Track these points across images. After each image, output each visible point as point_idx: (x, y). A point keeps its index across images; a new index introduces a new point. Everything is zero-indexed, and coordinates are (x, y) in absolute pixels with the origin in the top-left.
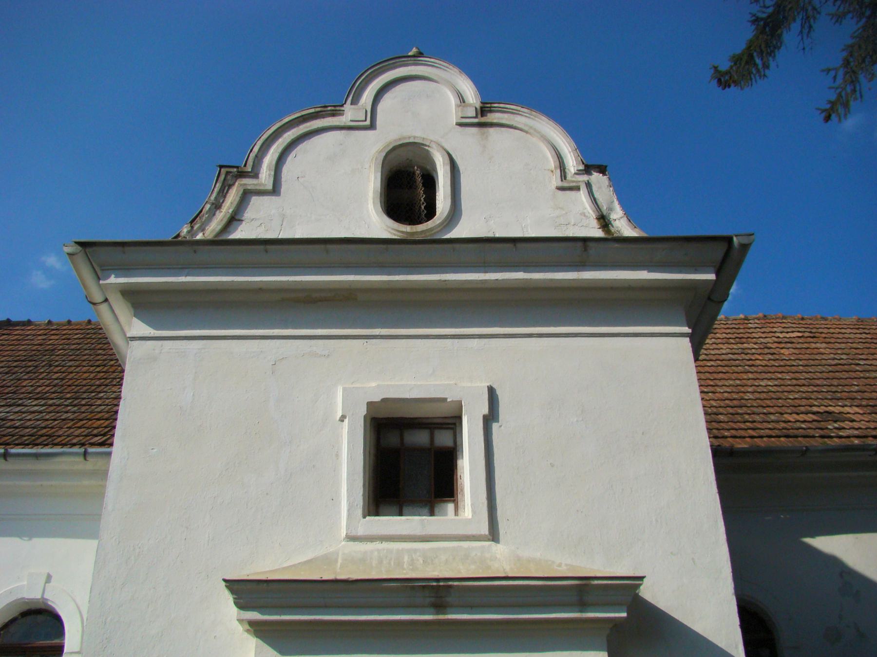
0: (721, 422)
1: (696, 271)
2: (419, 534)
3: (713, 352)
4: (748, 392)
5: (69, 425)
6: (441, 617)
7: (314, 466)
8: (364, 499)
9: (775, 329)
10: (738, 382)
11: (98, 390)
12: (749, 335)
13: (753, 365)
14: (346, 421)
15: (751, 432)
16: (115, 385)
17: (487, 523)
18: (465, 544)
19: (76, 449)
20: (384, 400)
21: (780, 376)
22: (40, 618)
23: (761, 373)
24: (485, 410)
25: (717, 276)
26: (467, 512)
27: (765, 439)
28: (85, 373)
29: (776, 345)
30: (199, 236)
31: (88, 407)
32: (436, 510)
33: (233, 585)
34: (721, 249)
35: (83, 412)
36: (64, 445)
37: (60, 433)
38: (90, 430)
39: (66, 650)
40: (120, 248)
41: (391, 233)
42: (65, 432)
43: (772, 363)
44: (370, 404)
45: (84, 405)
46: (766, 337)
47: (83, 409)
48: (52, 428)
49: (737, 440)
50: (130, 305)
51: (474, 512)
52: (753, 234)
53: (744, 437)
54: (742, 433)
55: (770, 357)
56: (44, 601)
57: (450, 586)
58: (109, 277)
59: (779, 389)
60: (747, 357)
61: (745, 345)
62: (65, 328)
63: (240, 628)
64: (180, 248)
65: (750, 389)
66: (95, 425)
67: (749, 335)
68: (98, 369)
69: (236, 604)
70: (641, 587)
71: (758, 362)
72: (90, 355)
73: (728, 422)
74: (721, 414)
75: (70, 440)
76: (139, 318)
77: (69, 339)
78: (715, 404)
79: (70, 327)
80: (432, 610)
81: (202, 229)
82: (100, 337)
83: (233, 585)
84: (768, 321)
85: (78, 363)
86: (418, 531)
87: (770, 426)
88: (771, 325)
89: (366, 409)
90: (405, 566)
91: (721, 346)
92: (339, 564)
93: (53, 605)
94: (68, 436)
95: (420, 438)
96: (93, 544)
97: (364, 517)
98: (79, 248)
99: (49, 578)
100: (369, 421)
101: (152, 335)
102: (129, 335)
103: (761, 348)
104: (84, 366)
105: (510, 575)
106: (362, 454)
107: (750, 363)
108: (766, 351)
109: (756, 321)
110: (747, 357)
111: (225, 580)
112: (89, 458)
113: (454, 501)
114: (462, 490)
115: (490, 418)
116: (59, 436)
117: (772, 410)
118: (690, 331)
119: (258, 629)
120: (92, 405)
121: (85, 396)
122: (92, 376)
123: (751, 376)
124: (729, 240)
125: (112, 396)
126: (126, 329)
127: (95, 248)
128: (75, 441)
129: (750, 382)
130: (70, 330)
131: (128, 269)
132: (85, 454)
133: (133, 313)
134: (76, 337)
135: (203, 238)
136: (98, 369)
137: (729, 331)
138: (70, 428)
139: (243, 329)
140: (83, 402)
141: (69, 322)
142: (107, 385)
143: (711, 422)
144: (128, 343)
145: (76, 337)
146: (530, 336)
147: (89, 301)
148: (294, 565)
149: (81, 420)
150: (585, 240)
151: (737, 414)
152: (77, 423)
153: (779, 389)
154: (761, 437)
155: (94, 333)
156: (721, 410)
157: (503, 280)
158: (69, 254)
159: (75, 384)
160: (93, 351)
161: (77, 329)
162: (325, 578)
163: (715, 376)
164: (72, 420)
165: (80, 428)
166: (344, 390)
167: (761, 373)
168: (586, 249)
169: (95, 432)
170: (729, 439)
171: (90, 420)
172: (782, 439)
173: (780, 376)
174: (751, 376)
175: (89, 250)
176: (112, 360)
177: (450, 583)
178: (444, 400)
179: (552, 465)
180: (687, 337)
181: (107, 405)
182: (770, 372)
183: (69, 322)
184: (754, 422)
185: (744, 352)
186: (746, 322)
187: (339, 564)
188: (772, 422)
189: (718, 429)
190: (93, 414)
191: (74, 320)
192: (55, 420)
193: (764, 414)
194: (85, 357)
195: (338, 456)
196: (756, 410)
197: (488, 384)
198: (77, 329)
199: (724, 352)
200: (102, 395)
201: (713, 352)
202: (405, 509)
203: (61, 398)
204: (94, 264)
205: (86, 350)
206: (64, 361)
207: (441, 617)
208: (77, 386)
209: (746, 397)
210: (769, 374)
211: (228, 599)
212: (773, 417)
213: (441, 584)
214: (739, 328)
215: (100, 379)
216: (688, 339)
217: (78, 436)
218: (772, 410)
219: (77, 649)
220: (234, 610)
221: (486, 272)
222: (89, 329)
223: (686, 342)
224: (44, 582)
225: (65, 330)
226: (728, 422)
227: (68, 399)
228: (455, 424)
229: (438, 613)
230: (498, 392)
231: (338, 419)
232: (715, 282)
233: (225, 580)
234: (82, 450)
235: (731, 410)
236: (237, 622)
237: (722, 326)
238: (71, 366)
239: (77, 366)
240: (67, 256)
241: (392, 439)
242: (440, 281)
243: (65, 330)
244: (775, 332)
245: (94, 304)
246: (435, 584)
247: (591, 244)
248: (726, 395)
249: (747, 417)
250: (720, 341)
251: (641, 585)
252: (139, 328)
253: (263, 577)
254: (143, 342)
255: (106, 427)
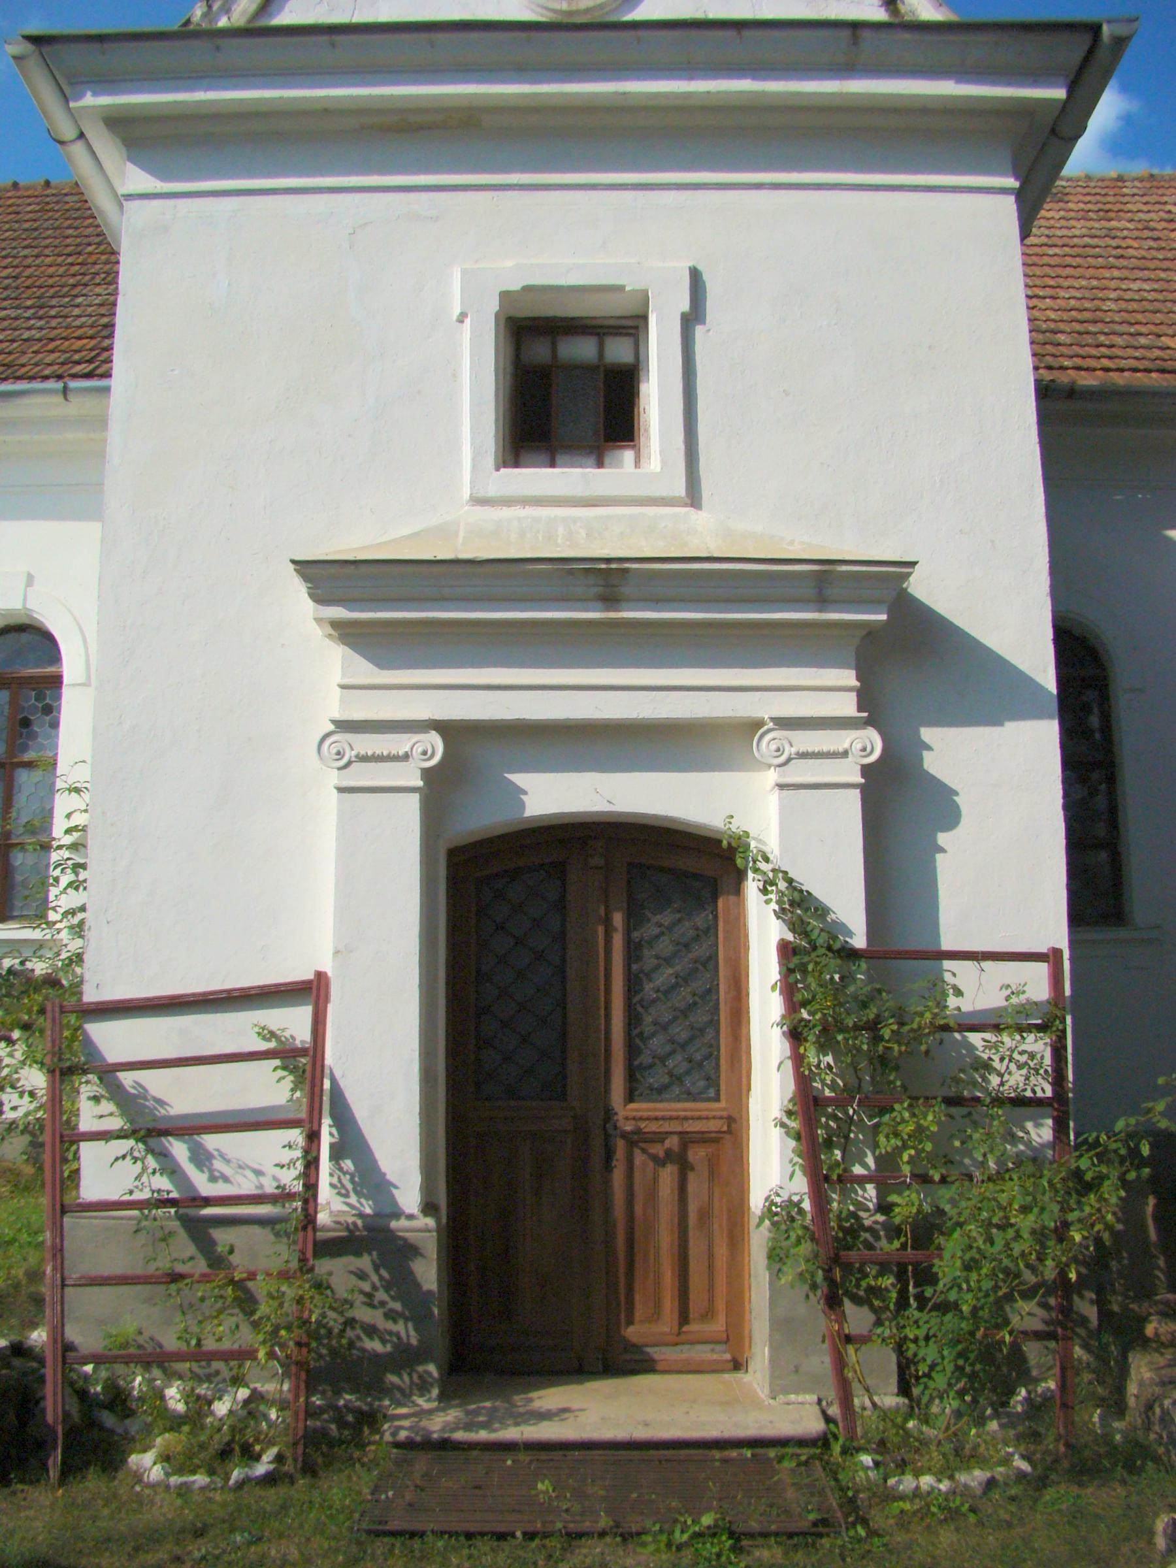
0: (1059, 344)
1: (1035, 84)
2: (580, 494)
3: (1059, 233)
4: (1108, 299)
5: (35, 348)
6: (612, 615)
7: (419, 392)
8: (496, 444)
9: (1165, 199)
10: (1095, 283)
11: (74, 292)
12: (1122, 207)
13: (1122, 257)
14: (468, 321)
15: (1106, 363)
16: (99, 284)
17: (684, 480)
18: (651, 511)
19: (51, 384)
20: (527, 289)
21: (1163, 275)
22: (25, 637)
23: (1133, 269)
24: (685, 306)
25: (1072, 89)
26: (654, 462)
27: (1126, 374)
28: (50, 266)
29: (1164, 224)
30: (223, 23)
31: (60, 320)
32: (607, 461)
33: (305, 568)
34: (1082, 43)
35: (55, 328)
36: (32, 378)
37: (23, 360)
38: (68, 355)
39: (66, 681)
40: (95, 46)
41: (532, 11)
42: (31, 359)
43: (1154, 253)
44: (505, 296)
45: (55, 317)
46: (1149, 212)
47: (54, 323)
48: (10, 353)
49: (1083, 373)
50: (118, 141)
51: (664, 463)
52: (1137, 19)
53: (1094, 370)
54: (1092, 363)
55: (1152, 243)
56: (28, 612)
57: (626, 570)
58: (84, 95)
59: (1160, 297)
60: (1114, 243)
61: (1114, 224)
62: (9, 194)
63: (318, 633)
64: (195, 43)
65: (1113, 295)
66: (74, 348)
67: (1122, 207)
68: (70, 260)
69: (311, 596)
70: (911, 579)
71: (1131, 252)
72: (55, 238)
73: (1071, 345)
74: (1062, 332)
75: (40, 371)
76: (135, 164)
77: (18, 213)
78: (1053, 317)
79: (19, 194)
80: (599, 604)
81: (226, 10)
82: (67, 207)
83: (305, 568)
84: (1155, 183)
85: (36, 251)
86: (579, 491)
87: (1137, 354)
88: (1160, 192)
89: (498, 303)
90: (559, 541)
91: (1073, 223)
92: (460, 540)
93: (42, 619)
94: (36, 365)
95: (582, 350)
96: (91, 531)
97: (498, 469)
98: (29, 47)
99: (30, 580)
100: (502, 322)
101: (158, 190)
102: (122, 191)
103: (1137, 229)
104: (48, 256)
105: (715, 555)
106: (493, 374)
107: (1119, 252)
108: (1146, 233)
109: (1137, 184)
110: (1114, 243)
111: (293, 562)
112: (71, 397)
113: (633, 447)
114: (647, 430)
115: (692, 319)
116: (23, 366)
117: (1143, 329)
118: (1017, 184)
119: (346, 633)
120: (66, 317)
121: (54, 302)
122: (61, 270)
123: (1116, 273)
124: (1094, 29)
125: (97, 301)
126: (116, 183)
127: (57, 47)
128: (47, 372)
129: (1113, 284)
130: (19, 197)
131: (113, 81)
132: (65, 391)
133: (125, 155)
134: (29, 209)
135: (229, 25)
136: (70, 260)
137: (1088, 198)
138: (36, 352)
139: (301, 176)
140: (53, 313)
141: (15, 185)
142: (86, 285)
143: (1033, 308)
144: (121, 206)
145: (29, 209)
146: (759, 186)
147: (55, 140)
148: (394, 541)
149: (52, 340)
150: (855, 26)
151: (1087, 333)
152: (46, 345)
153: (1160, 297)
154: (1122, 370)
155: (57, 203)
156: (1062, 326)
157: (718, 92)
158: (16, 58)
159: (38, 284)
160: (58, 232)
161: (29, 197)
162: (439, 558)
163: (1060, 271)
164: (40, 340)
165: (52, 351)
166: (464, 272)
167: (1133, 269)
168: (855, 41)
169: (76, 357)
170: (1070, 372)
171: (66, 339)
172: (1154, 375)
173: (1163, 275)
174: (1116, 273)
175: (46, 49)
176: (90, 245)
177: (627, 565)
178: (620, 289)
179: (786, 393)
180: (1011, 194)
181: (90, 316)
182: (1148, 269)
183: (15, 185)
184: (1112, 346)
185: (1110, 234)
186: (1120, 184)
187: (460, 540)
188: (1141, 347)
189: (1054, 356)
190: (70, 331)
191: (23, 182)
192: (13, 341)
193: (1131, 334)
194: (48, 241)
195: (455, 376)
196: (1117, 328)
197: (691, 264)
198: (29, 197)
199: (1077, 232)
200: (80, 300)
201: (1059, 233)
202: (560, 459)
203: (17, 308)
204: (56, 73)
205: (47, 229)
206: (14, 248)
207: (612, 615)
208: (40, 287)
209: (1104, 308)
210: (1146, 272)
211: (298, 589)
212: (1143, 341)
213: (614, 566)
214: (1106, 195)
215: (74, 275)
216: (1012, 198)
217: (49, 365)
218: (1143, 329)
219: (82, 680)
220: (310, 604)
221: (691, 79)
222: (47, 196)
223: (1009, 204)
224: (23, 586)
225: (10, 198)
226: (1071, 345)
227: (29, 308)
228: (636, 328)
229: (608, 610)
230: (706, 277)
231: (455, 318)
232: (1065, 105)
233: (293, 562)
234: (60, 385)
235: (1077, 327)
236: (314, 624)
237: (1079, 189)
238: (26, 257)
239: (37, 256)
240: (12, 61)
241: (539, 352)
242: (616, 93)
243: (10, 198)
244: (1166, 203)
245: (62, 143)
246: (603, 566)
247: (866, 34)
248: (1072, 302)
249: (1102, 338)
250: (1072, 214)
251: (909, 574)
252: (137, 179)
253: (351, 557)
254: (145, 202)
255: (91, 350)
